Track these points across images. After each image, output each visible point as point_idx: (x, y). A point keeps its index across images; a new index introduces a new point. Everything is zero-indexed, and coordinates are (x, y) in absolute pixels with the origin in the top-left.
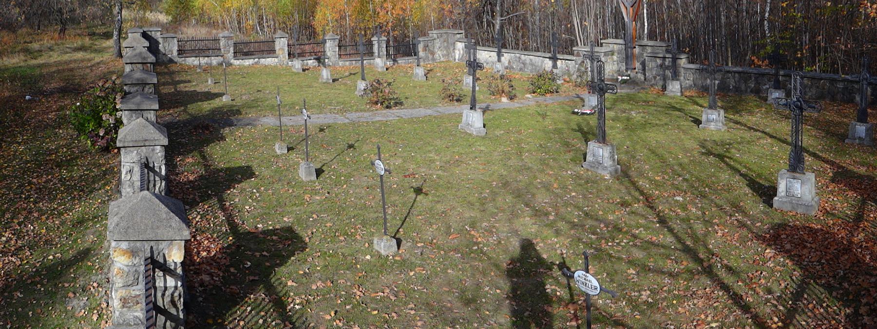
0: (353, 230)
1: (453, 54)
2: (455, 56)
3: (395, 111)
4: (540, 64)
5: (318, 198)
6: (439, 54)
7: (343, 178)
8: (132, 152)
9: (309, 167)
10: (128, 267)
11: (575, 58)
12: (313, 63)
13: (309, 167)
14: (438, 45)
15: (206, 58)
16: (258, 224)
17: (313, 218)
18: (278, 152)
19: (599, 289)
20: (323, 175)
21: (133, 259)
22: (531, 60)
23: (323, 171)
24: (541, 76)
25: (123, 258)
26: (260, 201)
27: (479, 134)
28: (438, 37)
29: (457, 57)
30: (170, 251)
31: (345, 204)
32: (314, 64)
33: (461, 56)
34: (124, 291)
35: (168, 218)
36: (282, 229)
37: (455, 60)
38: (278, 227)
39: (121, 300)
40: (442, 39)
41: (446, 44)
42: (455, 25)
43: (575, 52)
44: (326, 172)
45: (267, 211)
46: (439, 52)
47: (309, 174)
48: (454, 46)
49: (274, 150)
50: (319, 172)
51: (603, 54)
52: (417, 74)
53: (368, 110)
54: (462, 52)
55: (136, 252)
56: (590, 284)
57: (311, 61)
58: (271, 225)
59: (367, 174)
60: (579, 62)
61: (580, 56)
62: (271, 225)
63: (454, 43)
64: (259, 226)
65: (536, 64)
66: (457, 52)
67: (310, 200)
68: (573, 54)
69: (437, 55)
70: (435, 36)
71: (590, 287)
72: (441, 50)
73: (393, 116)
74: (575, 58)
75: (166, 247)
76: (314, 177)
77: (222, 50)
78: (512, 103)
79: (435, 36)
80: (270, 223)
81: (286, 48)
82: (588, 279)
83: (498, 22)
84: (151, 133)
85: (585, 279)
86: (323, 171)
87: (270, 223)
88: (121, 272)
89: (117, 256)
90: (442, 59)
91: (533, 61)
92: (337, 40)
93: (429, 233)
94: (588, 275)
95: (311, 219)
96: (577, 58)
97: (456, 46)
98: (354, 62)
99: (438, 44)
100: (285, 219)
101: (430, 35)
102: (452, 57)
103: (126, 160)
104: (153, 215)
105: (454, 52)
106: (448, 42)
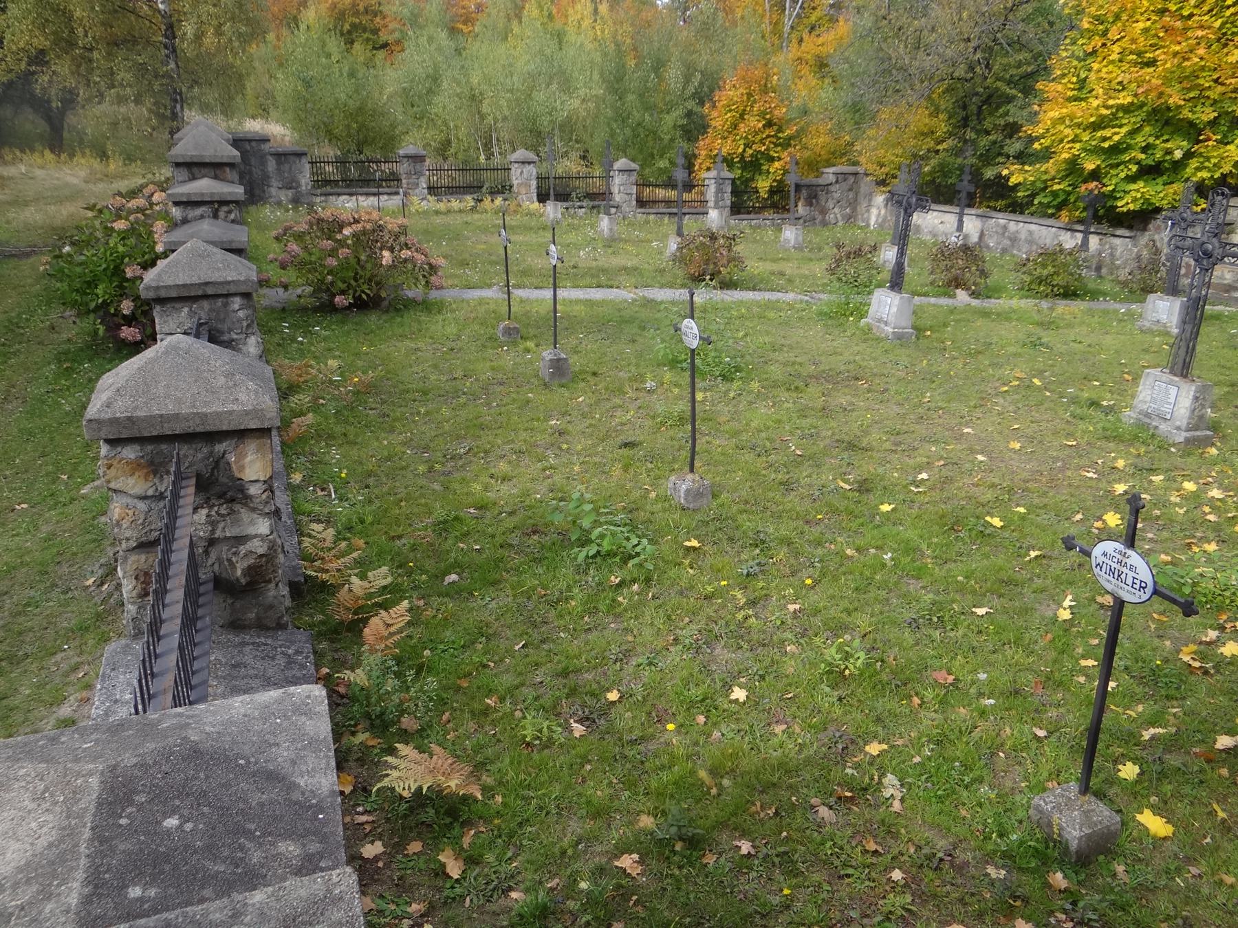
8: (179, 310)
10: (147, 502)
15: (372, 198)
19: (1149, 590)
21: (156, 480)
22: (1031, 233)
25: (131, 481)
28: (837, 182)
29: (872, 222)
30: (241, 457)
33: (880, 220)
34: (143, 557)
35: (231, 384)
39: (137, 578)
48: (870, 200)
55: (161, 464)
56: (1131, 574)
66: (874, 211)
71: (1129, 582)
75: (231, 449)
77: (404, 181)
81: (534, 183)
82: (1129, 562)
84: (219, 269)
85: (1119, 562)
88: (131, 513)
89: (117, 478)
91: (1036, 236)
94: (1130, 552)
97: (874, 199)
103: (166, 329)
104: (196, 381)
105: (868, 211)
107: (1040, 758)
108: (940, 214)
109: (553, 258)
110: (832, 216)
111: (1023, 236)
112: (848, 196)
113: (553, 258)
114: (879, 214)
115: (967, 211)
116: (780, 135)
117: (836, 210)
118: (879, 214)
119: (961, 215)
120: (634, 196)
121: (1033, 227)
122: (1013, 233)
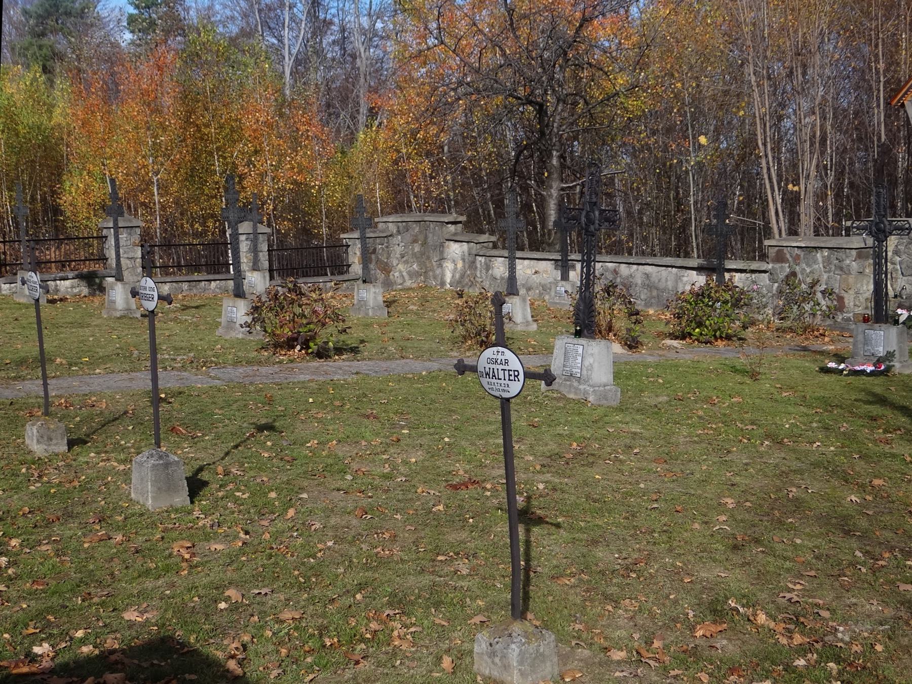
0: (374, 626)
1: (438, 271)
2: (443, 275)
3: (340, 363)
4: (670, 284)
5: (220, 547)
6: (401, 271)
7: (273, 495)
9: (167, 465)
11: (770, 266)
12: (72, 287)
13: (167, 465)
14: (398, 250)
16: (33, 643)
17: (227, 599)
18: (38, 449)
19: (521, 377)
20: (206, 491)
22: (647, 276)
23: (205, 484)
24: (703, 295)
26: (18, 577)
27: (604, 402)
28: (399, 232)
29: (448, 278)
31: (314, 557)
32: (76, 290)
33: (457, 276)
36: (130, 652)
37: (443, 284)
38: (112, 643)
40: (408, 237)
41: (417, 248)
42: (441, 206)
43: (772, 252)
44: (214, 486)
45: (56, 601)
46: (401, 267)
47: (165, 486)
48: (442, 253)
49: (21, 448)
50: (196, 486)
51: (854, 253)
52: (363, 303)
53: (267, 362)
54: (460, 265)
57: (68, 283)
58: (83, 641)
59: (339, 484)
60: (782, 276)
61: (786, 261)
62: (83, 641)
63: (442, 245)
64: (37, 650)
65: (662, 285)
66: (449, 266)
67: (193, 555)
68: (763, 257)
69: (397, 274)
70: (392, 228)
72: (406, 262)
73: (340, 372)
74: (770, 266)
76: (181, 498)
78: (636, 355)
79: (392, 228)
80: (80, 634)
83: (554, 192)
86: (205, 484)
87: (80, 634)
90: (408, 283)
91: (654, 279)
92: (138, 231)
93: (621, 622)
95: (223, 605)
96: (777, 266)
97: (446, 250)
98: (185, 286)
99: (398, 246)
100: (131, 615)
101: (380, 226)
102: (435, 278)
105: (440, 266)
106: (424, 243)
107: (206, 131)
108: (532, 262)
109: (150, 298)
110: (397, 274)
111: (639, 280)
112: (413, 249)
113: (150, 298)
114: (456, 268)
115: (519, 254)
116: (484, 619)
117: (400, 266)
118: (456, 268)
119: (512, 260)
120: (139, 261)
121: (649, 269)
122: (627, 278)
